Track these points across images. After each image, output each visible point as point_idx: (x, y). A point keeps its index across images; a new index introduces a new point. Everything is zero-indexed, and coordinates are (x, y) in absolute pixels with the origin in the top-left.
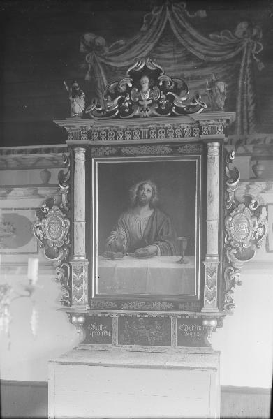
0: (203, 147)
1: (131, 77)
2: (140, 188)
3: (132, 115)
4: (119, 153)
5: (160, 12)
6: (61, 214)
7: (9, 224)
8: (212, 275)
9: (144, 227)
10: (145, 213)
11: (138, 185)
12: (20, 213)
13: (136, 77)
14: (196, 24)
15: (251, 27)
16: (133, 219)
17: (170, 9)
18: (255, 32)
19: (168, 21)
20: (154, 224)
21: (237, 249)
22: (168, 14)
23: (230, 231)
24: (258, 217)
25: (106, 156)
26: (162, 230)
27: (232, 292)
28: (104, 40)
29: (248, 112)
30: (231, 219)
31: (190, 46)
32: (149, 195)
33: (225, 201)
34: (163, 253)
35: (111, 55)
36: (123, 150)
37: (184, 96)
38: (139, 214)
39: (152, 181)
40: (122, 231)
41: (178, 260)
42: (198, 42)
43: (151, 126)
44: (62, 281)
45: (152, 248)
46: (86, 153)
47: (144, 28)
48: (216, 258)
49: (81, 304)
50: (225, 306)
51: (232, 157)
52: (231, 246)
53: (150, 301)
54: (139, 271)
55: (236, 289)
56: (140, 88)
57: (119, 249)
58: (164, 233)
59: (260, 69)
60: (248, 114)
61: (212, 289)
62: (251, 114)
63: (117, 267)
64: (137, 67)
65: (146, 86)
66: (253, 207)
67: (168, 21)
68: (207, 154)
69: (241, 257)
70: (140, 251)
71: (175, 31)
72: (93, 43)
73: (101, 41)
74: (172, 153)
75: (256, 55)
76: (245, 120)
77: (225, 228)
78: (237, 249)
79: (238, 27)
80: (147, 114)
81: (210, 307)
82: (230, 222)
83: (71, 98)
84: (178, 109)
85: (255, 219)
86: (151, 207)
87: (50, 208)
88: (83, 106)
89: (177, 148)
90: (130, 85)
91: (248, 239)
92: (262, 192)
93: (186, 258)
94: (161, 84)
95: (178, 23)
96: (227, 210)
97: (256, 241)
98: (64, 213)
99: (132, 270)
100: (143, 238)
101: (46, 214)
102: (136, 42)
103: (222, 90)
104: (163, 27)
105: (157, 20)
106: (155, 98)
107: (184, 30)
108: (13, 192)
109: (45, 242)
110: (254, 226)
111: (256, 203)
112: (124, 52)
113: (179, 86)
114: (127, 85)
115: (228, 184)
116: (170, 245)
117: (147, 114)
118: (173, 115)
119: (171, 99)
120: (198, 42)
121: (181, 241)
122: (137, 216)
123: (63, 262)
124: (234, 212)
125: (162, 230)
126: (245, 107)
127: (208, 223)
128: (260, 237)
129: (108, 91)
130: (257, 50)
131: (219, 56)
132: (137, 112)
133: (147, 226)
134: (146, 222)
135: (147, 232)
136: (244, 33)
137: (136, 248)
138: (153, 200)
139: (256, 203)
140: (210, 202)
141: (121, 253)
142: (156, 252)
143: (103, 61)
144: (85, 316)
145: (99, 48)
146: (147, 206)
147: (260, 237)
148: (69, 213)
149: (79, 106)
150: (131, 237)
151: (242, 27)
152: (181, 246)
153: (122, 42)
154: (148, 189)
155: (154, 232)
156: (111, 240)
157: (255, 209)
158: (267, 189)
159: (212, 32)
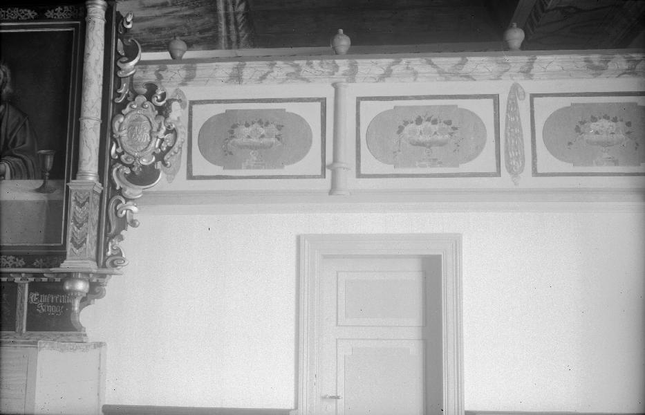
8: (81, 205)
21: (131, 166)
23: (120, 137)
24: (166, 117)
26: (16, 137)
27: (121, 239)
29: (236, 14)
30: (122, 119)
41: (38, 186)
50: (108, 261)
51: (128, 23)
52: (122, 163)
55: (127, 233)
58: (17, 144)
60: (235, 19)
62: (240, 18)
66: (158, 101)
69: (134, 179)
74: (36, 19)
76: (232, 27)
78: (131, 166)
81: (77, 260)
82: (121, 124)
85: (162, 118)
92: (183, 84)
93: (51, 183)
96: (112, 108)
110: (158, 130)
111: (164, 96)
115: (119, 64)
116: (24, 162)
121: (44, 156)
124: (128, 109)
125: (16, 137)
126: (231, 8)
128: (169, 149)
139: (164, 96)
147: (169, 149)
152: (44, 165)
157: (161, 104)
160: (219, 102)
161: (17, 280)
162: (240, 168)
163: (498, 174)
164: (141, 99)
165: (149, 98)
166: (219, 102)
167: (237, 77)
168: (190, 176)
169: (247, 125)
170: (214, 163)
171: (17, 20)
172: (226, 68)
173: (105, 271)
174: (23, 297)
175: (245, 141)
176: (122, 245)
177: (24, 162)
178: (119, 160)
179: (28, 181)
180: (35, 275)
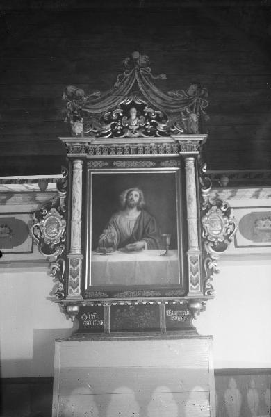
0: (182, 161)
1: (122, 109)
2: (129, 194)
3: (123, 136)
4: (111, 166)
5: (129, 74)
6: (59, 215)
7: (6, 226)
8: (194, 263)
9: (133, 226)
10: (134, 214)
11: (127, 192)
12: (17, 217)
13: (126, 109)
14: (158, 83)
15: (199, 88)
16: (123, 219)
17: (138, 71)
18: (203, 92)
19: (136, 82)
20: (141, 224)
22: (137, 76)
24: (228, 217)
25: (98, 168)
26: (149, 228)
27: (212, 279)
28: (83, 92)
30: (206, 218)
31: (152, 99)
32: (136, 199)
33: (201, 204)
34: (149, 248)
35: (87, 104)
36: (115, 163)
37: (164, 123)
38: (128, 214)
39: (139, 189)
40: (113, 230)
42: (158, 96)
43: (138, 145)
44: (58, 274)
45: (140, 244)
46: (83, 165)
47: (116, 84)
48: (197, 249)
49: (75, 293)
50: (207, 291)
53: (137, 290)
54: (129, 264)
55: (214, 276)
56: (129, 117)
57: (110, 245)
59: (207, 120)
61: (196, 275)
63: (109, 261)
64: (126, 102)
65: (134, 115)
67: (136, 82)
68: (185, 166)
70: (129, 246)
71: (141, 88)
72: (73, 94)
73: (80, 92)
75: (203, 109)
77: (202, 226)
78: (213, 242)
79: (190, 88)
80: (135, 135)
81: (194, 291)
83: (72, 122)
84: (160, 133)
86: (139, 209)
87: (49, 210)
88: (82, 128)
89: (159, 162)
90: (121, 115)
91: (222, 234)
92: (228, 199)
93: (170, 252)
94: (146, 115)
95: (143, 82)
96: (202, 213)
97: (229, 235)
98: (61, 215)
99: (122, 263)
100: (132, 235)
101: (45, 215)
102: (109, 95)
103: (195, 120)
104: (132, 85)
105: (127, 80)
106: (141, 125)
107: (148, 88)
108: (13, 198)
109: (42, 240)
112: (99, 101)
113: (160, 116)
114: (118, 114)
116: (155, 240)
117: (135, 135)
118: (156, 136)
119: (155, 125)
120: (158, 96)
121: (165, 237)
122: (127, 217)
123: (58, 258)
127: (188, 220)
128: (231, 233)
129: (102, 118)
130: (205, 104)
131: (175, 108)
132: (128, 134)
133: (135, 225)
134: (135, 222)
135: (135, 230)
136: (195, 92)
137: (125, 244)
138: (141, 203)
140: (189, 203)
141: (112, 249)
142: (144, 247)
143: (80, 107)
144: (78, 303)
145: (79, 98)
146: (135, 208)
147: (231, 233)
148: (67, 216)
149: (78, 128)
150: (121, 234)
151: (192, 89)
152: (165, 242)
153: (97, 94)
154: (136, 195)
155: (142, 229)
156: (103, 237)
158: (232, 196)
159: (169, 90)
160: (247, 208)
161: (159, 303)
162: (261, 241)
163: (32, 252)
164: (215, 208)
165: (219, 208)
166: (247, 208)
167: (256, 196)
168: (236, 246)
169: (263, 220)
170: (249, 239)
171: (146, 167)
172: (252, 191)
173: (205, 297)
174: (163, 313)
175: (262, 228)
176: (211, 283)
177: (155, 240)
178: (207, 239)
179: (157, 251)
180: (169, 301)
